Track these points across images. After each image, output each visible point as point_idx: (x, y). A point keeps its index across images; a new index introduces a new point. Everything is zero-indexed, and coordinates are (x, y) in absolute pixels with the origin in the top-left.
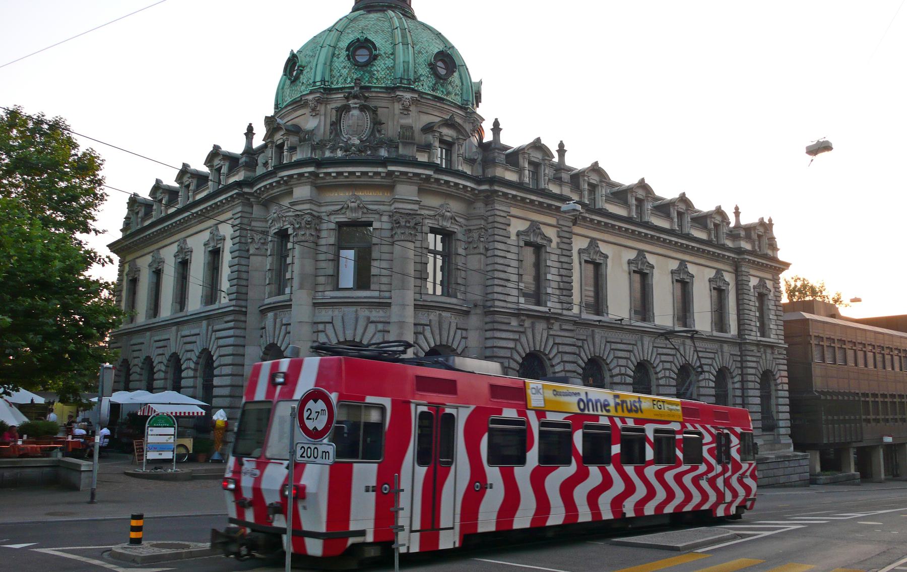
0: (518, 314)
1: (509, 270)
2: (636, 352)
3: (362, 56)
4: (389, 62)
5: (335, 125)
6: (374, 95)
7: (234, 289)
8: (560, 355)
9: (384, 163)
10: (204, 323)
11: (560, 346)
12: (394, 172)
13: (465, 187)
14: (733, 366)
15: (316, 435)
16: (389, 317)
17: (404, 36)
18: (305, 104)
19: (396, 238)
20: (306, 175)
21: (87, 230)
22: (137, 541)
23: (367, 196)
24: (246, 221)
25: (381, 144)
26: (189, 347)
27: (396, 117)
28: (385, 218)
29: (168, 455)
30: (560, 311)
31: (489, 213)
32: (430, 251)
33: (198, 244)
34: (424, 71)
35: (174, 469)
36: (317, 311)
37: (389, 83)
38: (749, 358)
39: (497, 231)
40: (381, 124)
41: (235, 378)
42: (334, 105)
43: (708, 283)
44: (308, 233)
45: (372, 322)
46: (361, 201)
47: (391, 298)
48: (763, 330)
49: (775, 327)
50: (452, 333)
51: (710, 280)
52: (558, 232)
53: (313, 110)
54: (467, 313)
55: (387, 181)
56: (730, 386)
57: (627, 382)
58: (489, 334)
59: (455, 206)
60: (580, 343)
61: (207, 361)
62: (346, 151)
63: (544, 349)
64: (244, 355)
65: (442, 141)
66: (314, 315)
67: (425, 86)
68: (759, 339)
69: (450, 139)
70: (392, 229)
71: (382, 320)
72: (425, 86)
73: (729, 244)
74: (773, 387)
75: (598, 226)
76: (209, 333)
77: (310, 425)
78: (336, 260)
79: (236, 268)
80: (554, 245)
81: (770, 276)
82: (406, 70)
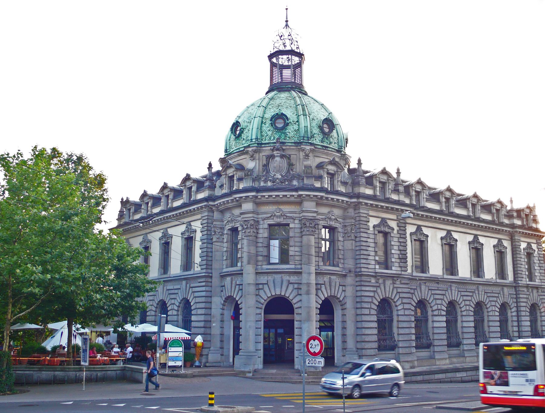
0: (376, 276)
1: (370, 249)
2: (447, 295)
3: (280, 124)
4: (296, 127)
5: (266, 166)
6: (288, 147)
7: (204, 262)
8: (400, 299)
9: (296, 190)
10: (184, 282)
11: (401, 294)
12: (302, 195)
13: (343, 201)
14: (511, 302)
15: (315, 354)
16: (301, 280)
17: (303, 110)
18: (247, 153)
19: (304, 233)
20: (251, 197)
21: (100, 222)
22: (211, 405)
23: (286, 209)
24: (210, 221)
25: (293, 178)
26: (173, 296)
27: (301, 161)
28: (297, 221)
29: (179, 363)
30: (400, 272)
31: (356, 215)
32: (323, 240)
33: (177, 232)
34: (316, 131)
35: (183, 371)
36: (258, 277)
37: (296, 140)
38: (521, 296)
39: (362, 226)
40: (293, 165)
41: (206, 316)
42: (264, 154)
43: (493, 248)
44: (252, 231)
45: (291, 283)
46: (283, 212)
47: (301, 269)
48: (531, 277)
49: (539, 275)
50: (337, 288)
51: (494, 246)
52: (398, 223)
53: (252, 156)
54: (345, 276)
55: (298, 200)
56: (509, 314)
57: (442, 314)
58: (358, 288)
59: (337, 212)
60: (412, 292)
61: (186, 305)
62: (273, 182)
63: (391, 296)
64: (211, 302)
65: (328, 173)
66: (256, 280)
67: (317, 140)
68: (528, 283)
69: (333, 172)
70: (301, 228)
71: (297, 282)
72: (317, 140)
73: (506, 221)
74: (538, 314)
75: (422, 218)
76: (188, 289)
77: (312, 350)
78: (268, 247)
79: (205, 250)
80: (395, 232)
81: (534, 241)
82: (306, 132)
